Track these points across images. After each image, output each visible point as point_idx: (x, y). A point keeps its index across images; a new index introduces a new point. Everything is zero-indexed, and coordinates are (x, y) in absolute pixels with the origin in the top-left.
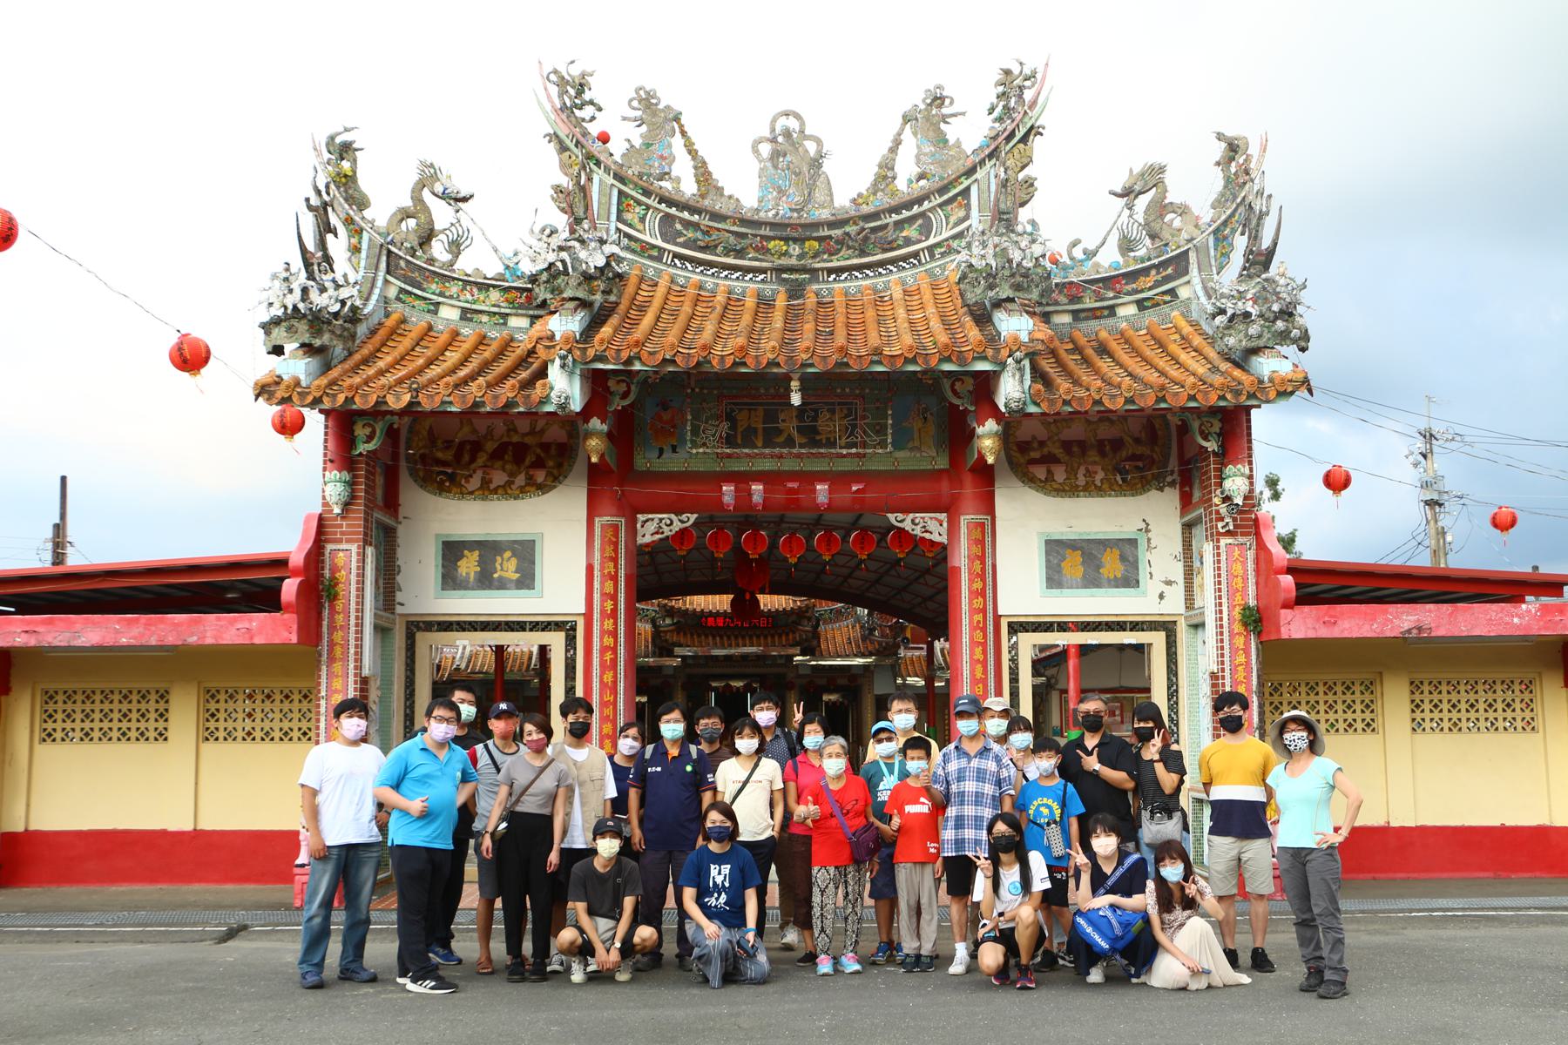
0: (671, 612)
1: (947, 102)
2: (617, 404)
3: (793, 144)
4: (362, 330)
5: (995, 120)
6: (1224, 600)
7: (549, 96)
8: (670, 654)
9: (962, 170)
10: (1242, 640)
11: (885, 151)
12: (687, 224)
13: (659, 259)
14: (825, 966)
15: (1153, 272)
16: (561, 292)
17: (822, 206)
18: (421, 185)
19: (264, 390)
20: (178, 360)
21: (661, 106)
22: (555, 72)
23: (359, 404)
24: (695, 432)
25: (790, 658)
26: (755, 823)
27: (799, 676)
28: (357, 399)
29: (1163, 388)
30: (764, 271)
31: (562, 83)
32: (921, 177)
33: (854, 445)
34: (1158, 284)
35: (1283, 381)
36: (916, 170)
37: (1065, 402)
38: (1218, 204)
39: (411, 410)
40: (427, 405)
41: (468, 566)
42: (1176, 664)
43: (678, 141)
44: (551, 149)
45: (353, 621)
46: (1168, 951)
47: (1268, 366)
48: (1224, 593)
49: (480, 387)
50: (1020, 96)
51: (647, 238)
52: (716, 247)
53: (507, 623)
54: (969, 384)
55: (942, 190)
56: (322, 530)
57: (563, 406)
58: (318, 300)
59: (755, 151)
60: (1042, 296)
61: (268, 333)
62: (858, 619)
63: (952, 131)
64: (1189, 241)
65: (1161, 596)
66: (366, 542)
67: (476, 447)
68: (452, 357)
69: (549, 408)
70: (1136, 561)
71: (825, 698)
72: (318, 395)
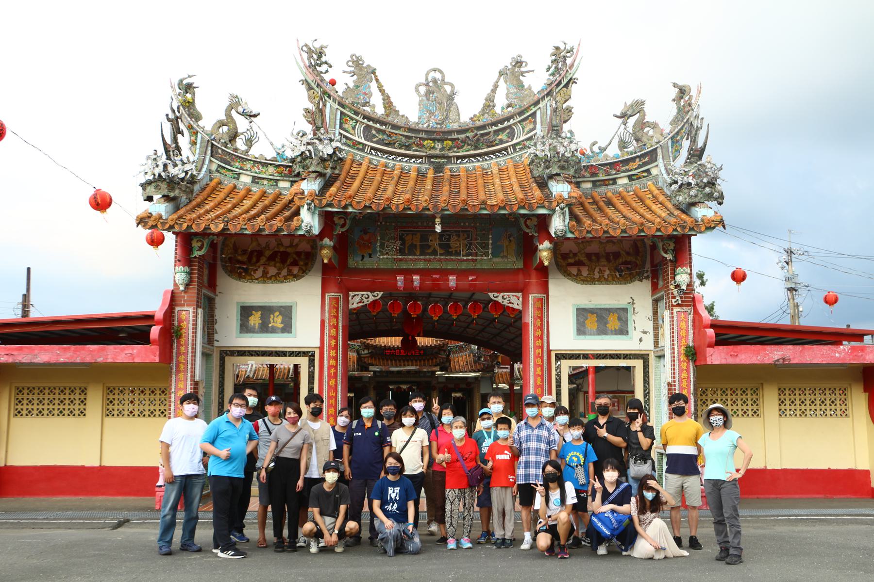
0: (367, 346)
1: (524, 64)
2: (339, 231)
3: (438, 87)
4: (197, 188)
5: (550, 75)
6: (676, 343)
7: (302, 59)
8: (367, 370)
9: (532, 102)
10: (685, 364)
11: (489, 91)
12: (379, 131)
13: (363, 150)
14: (452, 544)
15: (638, 160)
16: (308, 168)
17: (454, 122)
18: (230, 108)
19: (142, 221)
20: (94, 203)
21: (365, 65)
22: (306, 45)
23: (195, 229)
24: (382, 246)
25: (434, 372)
26: (413, 464)
27: (439, 383)
28: (194, 226)
29: (642, 224)
30: (421, 157)
31: (310, 52)
32: (509, 106)
33: (471, 255)
34: (640, 167)
35: (709, 221)
36: (506, 102)
37: (588, 232)
38: (673, 122)
39: (224, 233)
40: (233, 230)
41: (255, 320)
42: (648, 378)
43: (374, 85)
44: (303, 88)
45: (190, 350)
46: (643, 537)
47: (701, 212)
48: (676, 339)
49: (262, 221)
50: (564, 62)
51: (356, 138)
52: (394, 143)
53: (276, 352)
54: (535, 221)
55: (521, 113)
56: (173, 300)
57: (309, 232)
58: (173, 171)
59: (417, 90)
60: (575, 172)
61: (144, 189)
62: (472, 351)
63: (526, 80)
64: (657, 143)
65: (641, 340)
66: (198, 306)
67: (260, 254)
68: (247, 203)
69: (301, 232)
70: (627, 321)
71: (453, 395)
72: (172, 224)
